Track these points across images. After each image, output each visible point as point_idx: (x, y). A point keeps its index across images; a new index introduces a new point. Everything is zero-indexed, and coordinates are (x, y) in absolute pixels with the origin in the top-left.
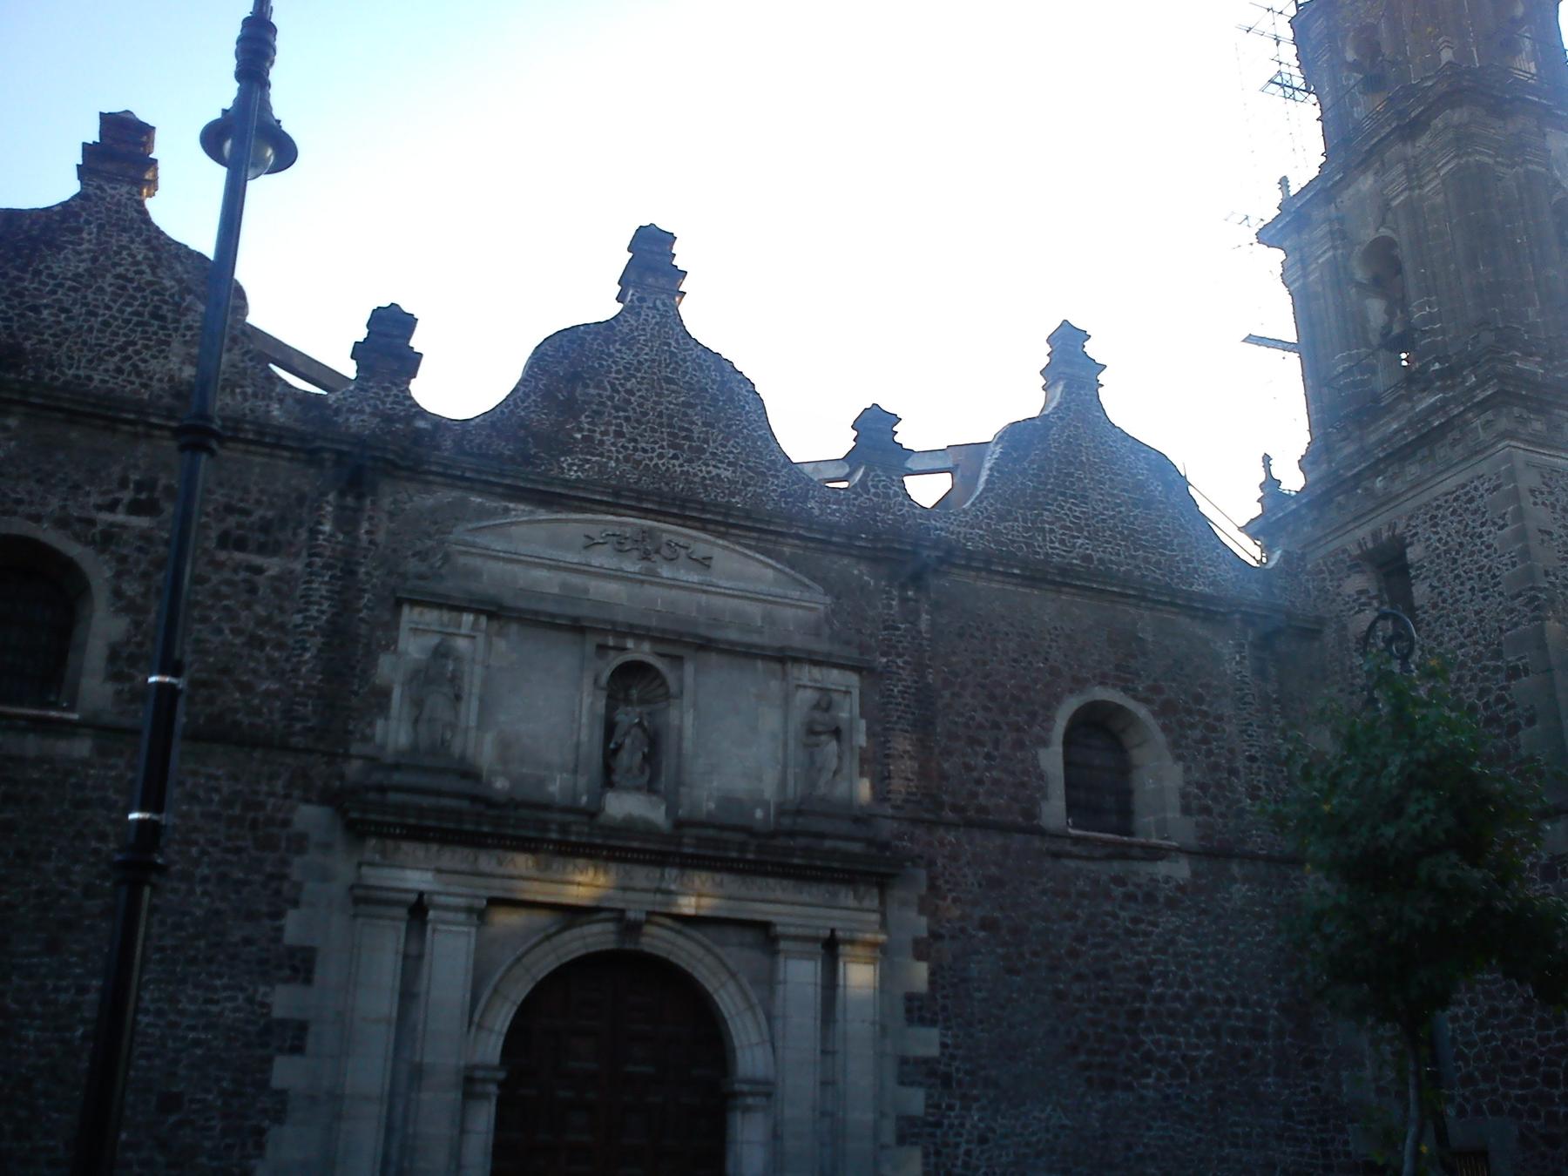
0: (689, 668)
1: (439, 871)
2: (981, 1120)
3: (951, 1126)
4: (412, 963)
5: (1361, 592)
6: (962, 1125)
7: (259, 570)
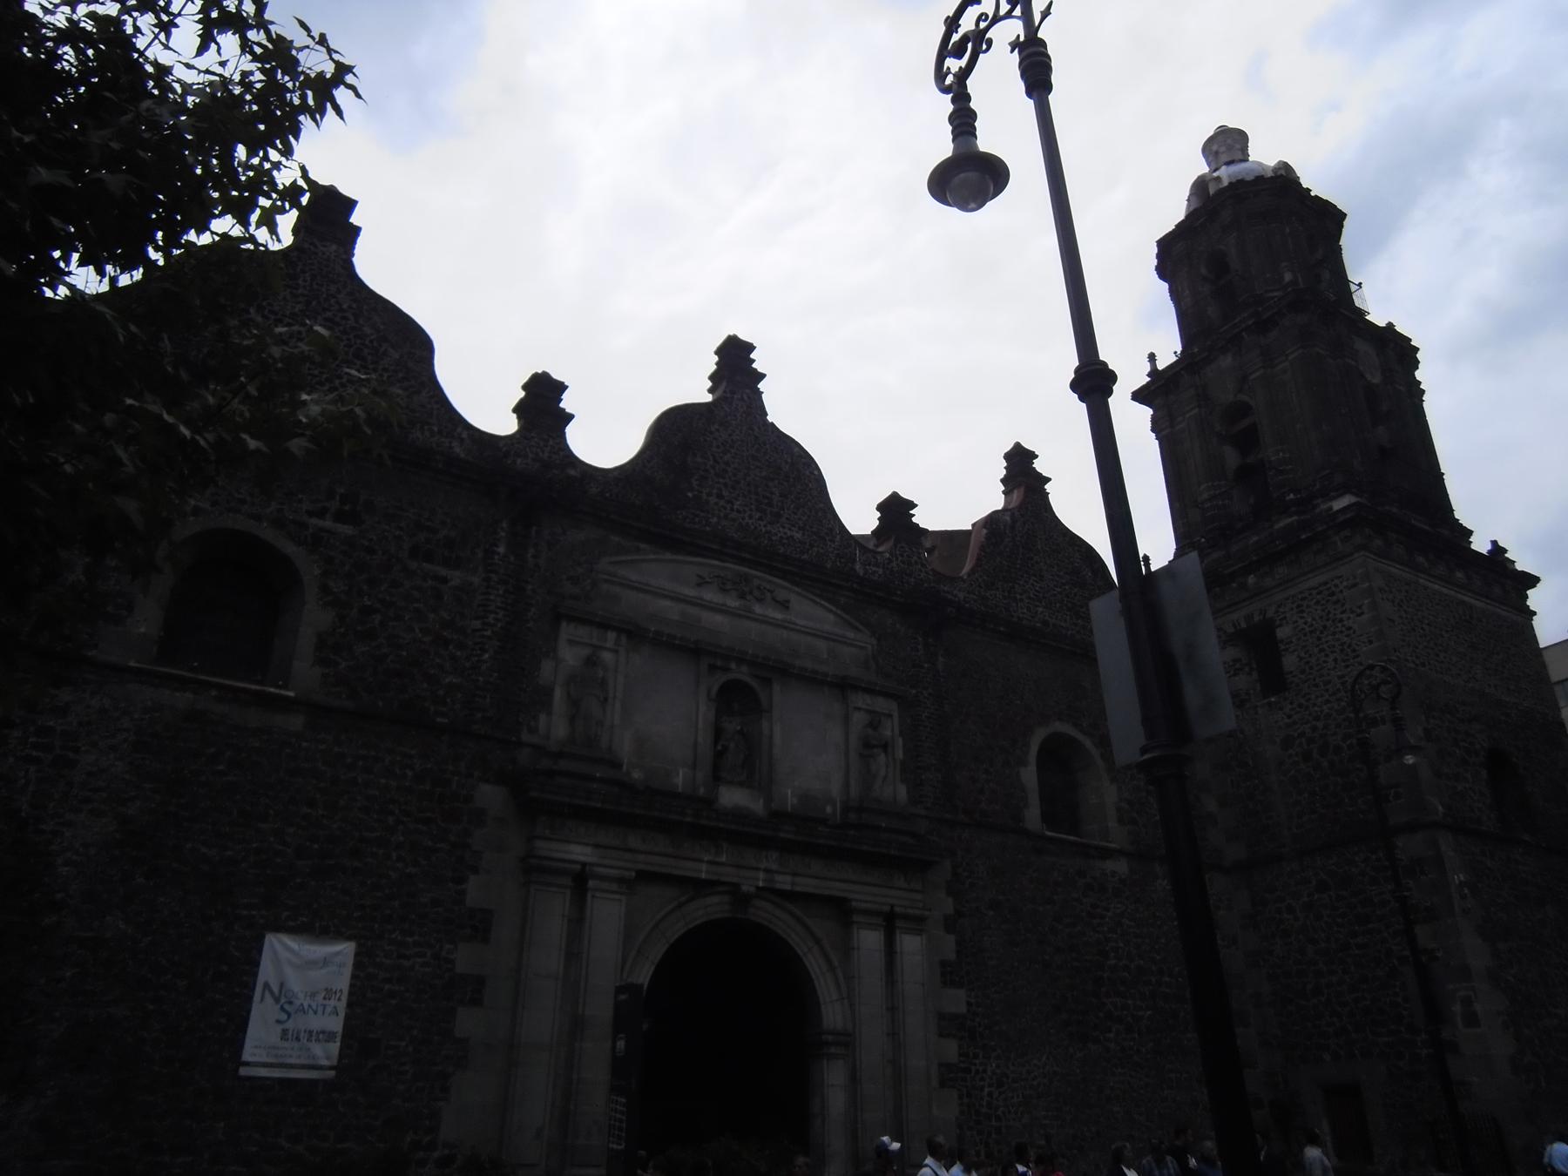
0: (776, 688)
1: (597, 846)
2: (998, 1066)
3: (977, 1072)
4: (577, 922)
5: (1235, 661)
6: (985, 1071)
7: (445, 580)
